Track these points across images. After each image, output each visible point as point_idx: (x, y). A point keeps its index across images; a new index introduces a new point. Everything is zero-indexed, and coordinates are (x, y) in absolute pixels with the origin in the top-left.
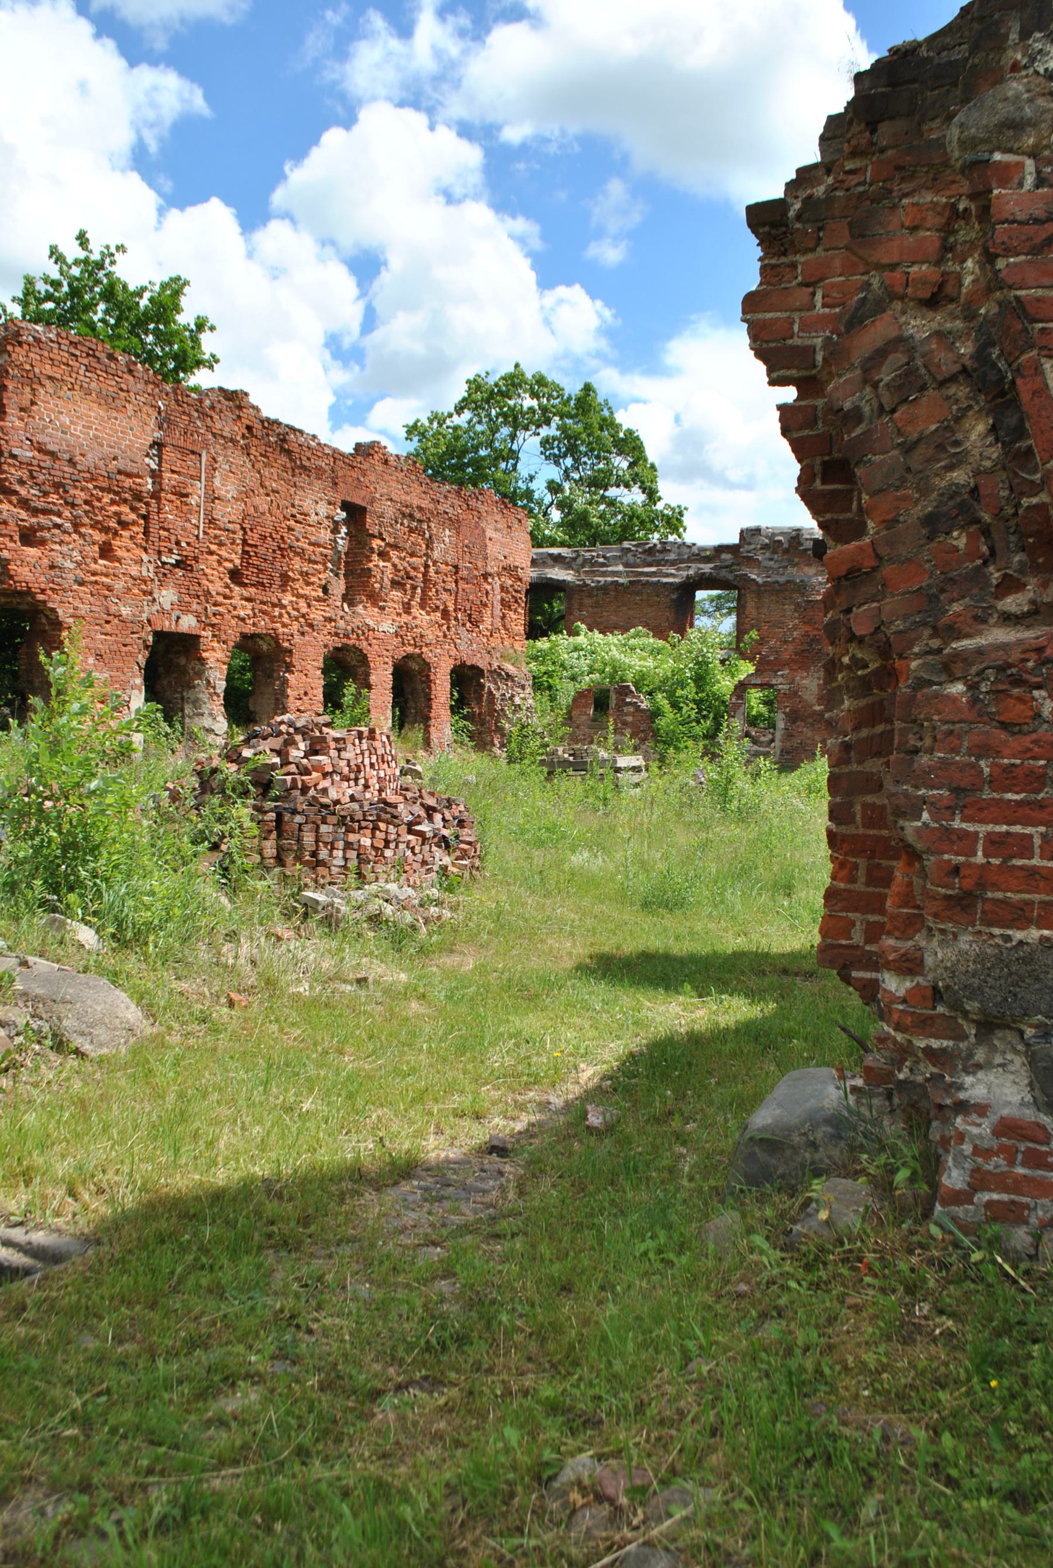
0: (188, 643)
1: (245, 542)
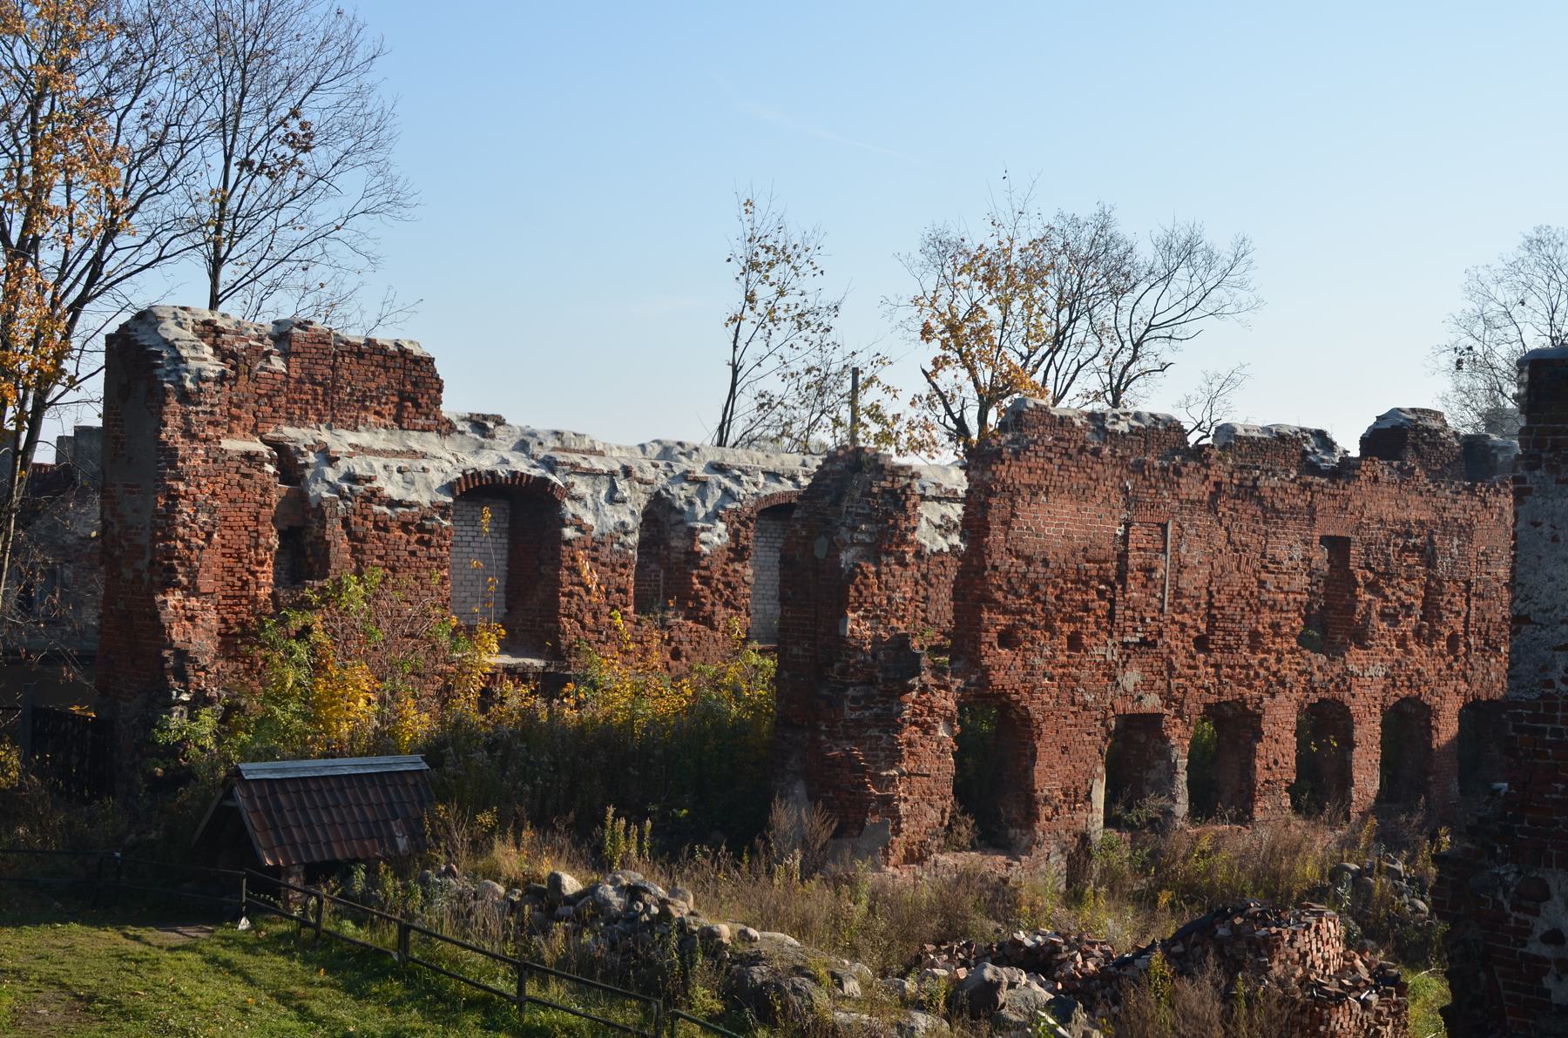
0: (1152, 722)
1: (1210, 605)
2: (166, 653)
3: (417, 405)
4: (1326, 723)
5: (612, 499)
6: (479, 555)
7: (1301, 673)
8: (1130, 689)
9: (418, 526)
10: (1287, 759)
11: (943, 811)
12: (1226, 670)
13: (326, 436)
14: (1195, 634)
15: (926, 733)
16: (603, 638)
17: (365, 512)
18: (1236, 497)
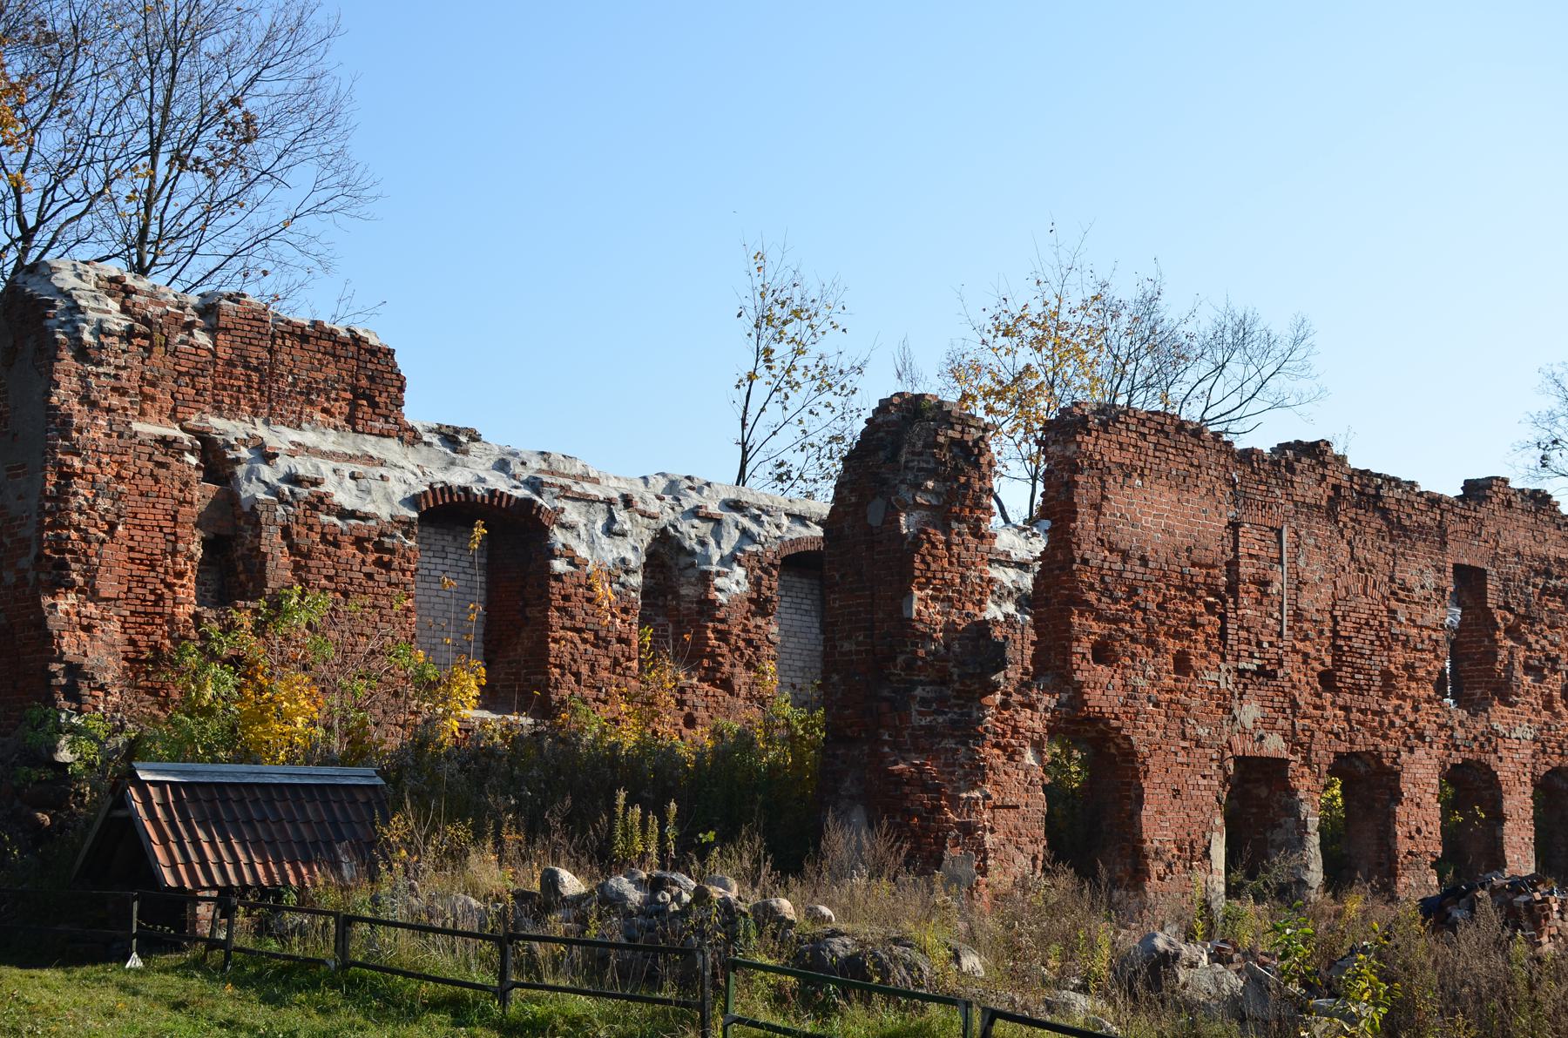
2: (55, 667)
3: (374, 405)
4: (1470, 787)
5: (609, 531)
6: (452, 585)
7: (1441, 727)
8: (1250, 726)
9: (375, 544)
10: (1431, 828)
11: (1035, 858)
12: (1355, 715)
13: (262, 431)
14: (1321, 668)
15: (1011, 758)
16: (602, 696)
17: (310, 521)
18: (1358, 506)
